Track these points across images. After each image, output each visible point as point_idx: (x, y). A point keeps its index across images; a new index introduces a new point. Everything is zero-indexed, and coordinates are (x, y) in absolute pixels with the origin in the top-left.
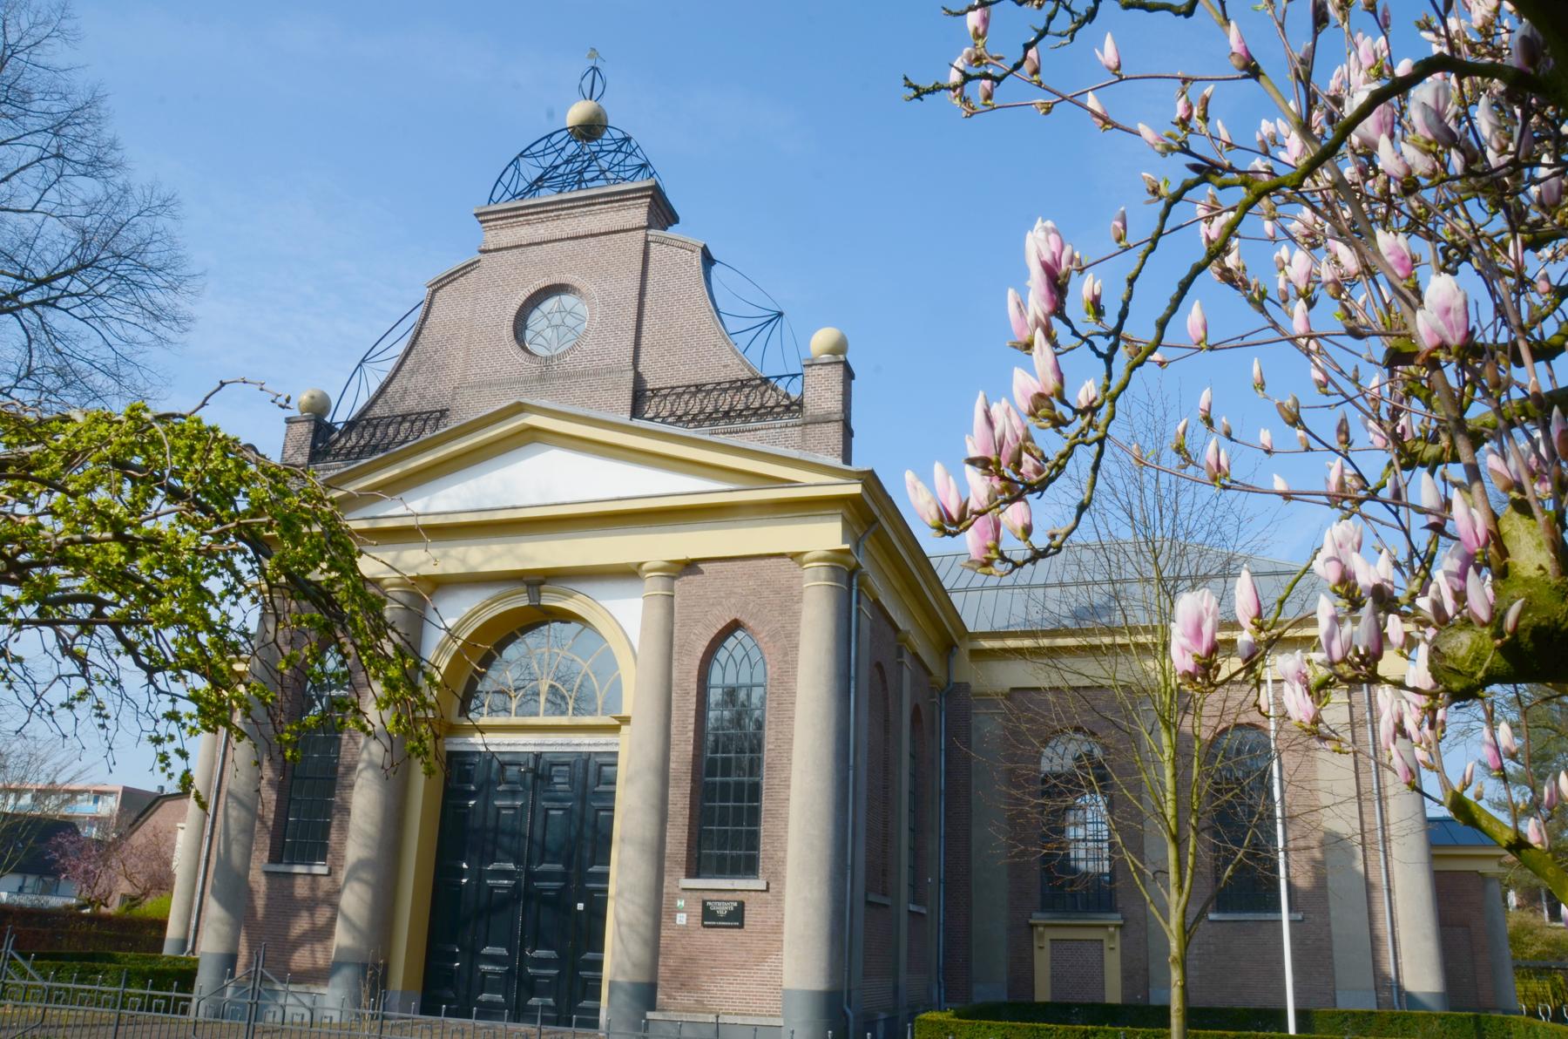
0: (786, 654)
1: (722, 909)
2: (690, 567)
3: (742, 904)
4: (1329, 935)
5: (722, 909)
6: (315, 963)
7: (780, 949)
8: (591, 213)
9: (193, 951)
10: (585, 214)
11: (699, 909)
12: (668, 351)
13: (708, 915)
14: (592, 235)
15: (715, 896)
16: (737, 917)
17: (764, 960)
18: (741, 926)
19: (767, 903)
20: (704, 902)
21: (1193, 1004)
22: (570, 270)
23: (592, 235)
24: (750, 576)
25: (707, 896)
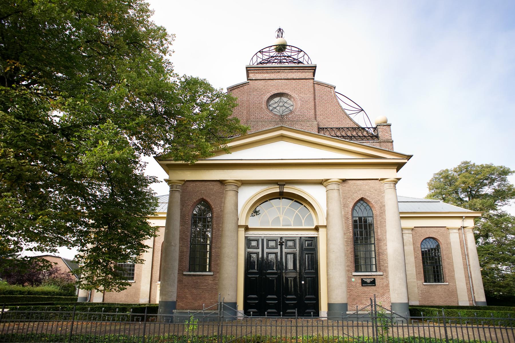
0: (381, 208)
1: (368, 281)
2: (344, 181)
3: (374, 279)
4: (456, 288)
5: (368, 281)
6: (166, 203)
7: (389, 292)
8: (292, 72)
9: (90, 301)
10: (289, 72)
11: (360, 281)
12: (327, 117)
13: (364, 283)
14: (293, 79)
15: (365, 277)
16: (373, 283)
17: (384, 295)
18: (375, 285)
19: (383, 279)
20: (362, 279)
21: (332, 301)
22: (286, 89)
23: (293, 79)
24: (366, 185)
25: (362, 277)
